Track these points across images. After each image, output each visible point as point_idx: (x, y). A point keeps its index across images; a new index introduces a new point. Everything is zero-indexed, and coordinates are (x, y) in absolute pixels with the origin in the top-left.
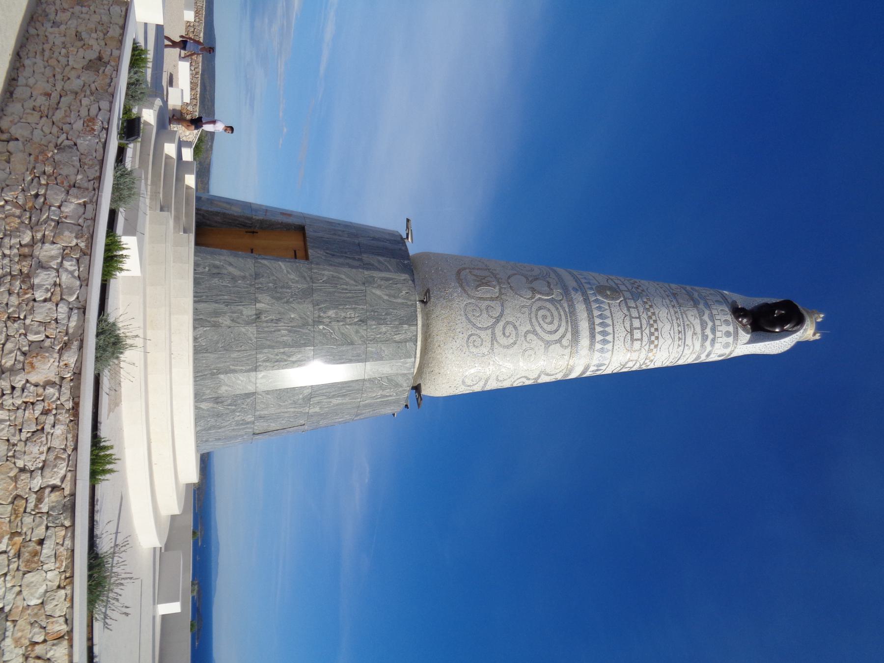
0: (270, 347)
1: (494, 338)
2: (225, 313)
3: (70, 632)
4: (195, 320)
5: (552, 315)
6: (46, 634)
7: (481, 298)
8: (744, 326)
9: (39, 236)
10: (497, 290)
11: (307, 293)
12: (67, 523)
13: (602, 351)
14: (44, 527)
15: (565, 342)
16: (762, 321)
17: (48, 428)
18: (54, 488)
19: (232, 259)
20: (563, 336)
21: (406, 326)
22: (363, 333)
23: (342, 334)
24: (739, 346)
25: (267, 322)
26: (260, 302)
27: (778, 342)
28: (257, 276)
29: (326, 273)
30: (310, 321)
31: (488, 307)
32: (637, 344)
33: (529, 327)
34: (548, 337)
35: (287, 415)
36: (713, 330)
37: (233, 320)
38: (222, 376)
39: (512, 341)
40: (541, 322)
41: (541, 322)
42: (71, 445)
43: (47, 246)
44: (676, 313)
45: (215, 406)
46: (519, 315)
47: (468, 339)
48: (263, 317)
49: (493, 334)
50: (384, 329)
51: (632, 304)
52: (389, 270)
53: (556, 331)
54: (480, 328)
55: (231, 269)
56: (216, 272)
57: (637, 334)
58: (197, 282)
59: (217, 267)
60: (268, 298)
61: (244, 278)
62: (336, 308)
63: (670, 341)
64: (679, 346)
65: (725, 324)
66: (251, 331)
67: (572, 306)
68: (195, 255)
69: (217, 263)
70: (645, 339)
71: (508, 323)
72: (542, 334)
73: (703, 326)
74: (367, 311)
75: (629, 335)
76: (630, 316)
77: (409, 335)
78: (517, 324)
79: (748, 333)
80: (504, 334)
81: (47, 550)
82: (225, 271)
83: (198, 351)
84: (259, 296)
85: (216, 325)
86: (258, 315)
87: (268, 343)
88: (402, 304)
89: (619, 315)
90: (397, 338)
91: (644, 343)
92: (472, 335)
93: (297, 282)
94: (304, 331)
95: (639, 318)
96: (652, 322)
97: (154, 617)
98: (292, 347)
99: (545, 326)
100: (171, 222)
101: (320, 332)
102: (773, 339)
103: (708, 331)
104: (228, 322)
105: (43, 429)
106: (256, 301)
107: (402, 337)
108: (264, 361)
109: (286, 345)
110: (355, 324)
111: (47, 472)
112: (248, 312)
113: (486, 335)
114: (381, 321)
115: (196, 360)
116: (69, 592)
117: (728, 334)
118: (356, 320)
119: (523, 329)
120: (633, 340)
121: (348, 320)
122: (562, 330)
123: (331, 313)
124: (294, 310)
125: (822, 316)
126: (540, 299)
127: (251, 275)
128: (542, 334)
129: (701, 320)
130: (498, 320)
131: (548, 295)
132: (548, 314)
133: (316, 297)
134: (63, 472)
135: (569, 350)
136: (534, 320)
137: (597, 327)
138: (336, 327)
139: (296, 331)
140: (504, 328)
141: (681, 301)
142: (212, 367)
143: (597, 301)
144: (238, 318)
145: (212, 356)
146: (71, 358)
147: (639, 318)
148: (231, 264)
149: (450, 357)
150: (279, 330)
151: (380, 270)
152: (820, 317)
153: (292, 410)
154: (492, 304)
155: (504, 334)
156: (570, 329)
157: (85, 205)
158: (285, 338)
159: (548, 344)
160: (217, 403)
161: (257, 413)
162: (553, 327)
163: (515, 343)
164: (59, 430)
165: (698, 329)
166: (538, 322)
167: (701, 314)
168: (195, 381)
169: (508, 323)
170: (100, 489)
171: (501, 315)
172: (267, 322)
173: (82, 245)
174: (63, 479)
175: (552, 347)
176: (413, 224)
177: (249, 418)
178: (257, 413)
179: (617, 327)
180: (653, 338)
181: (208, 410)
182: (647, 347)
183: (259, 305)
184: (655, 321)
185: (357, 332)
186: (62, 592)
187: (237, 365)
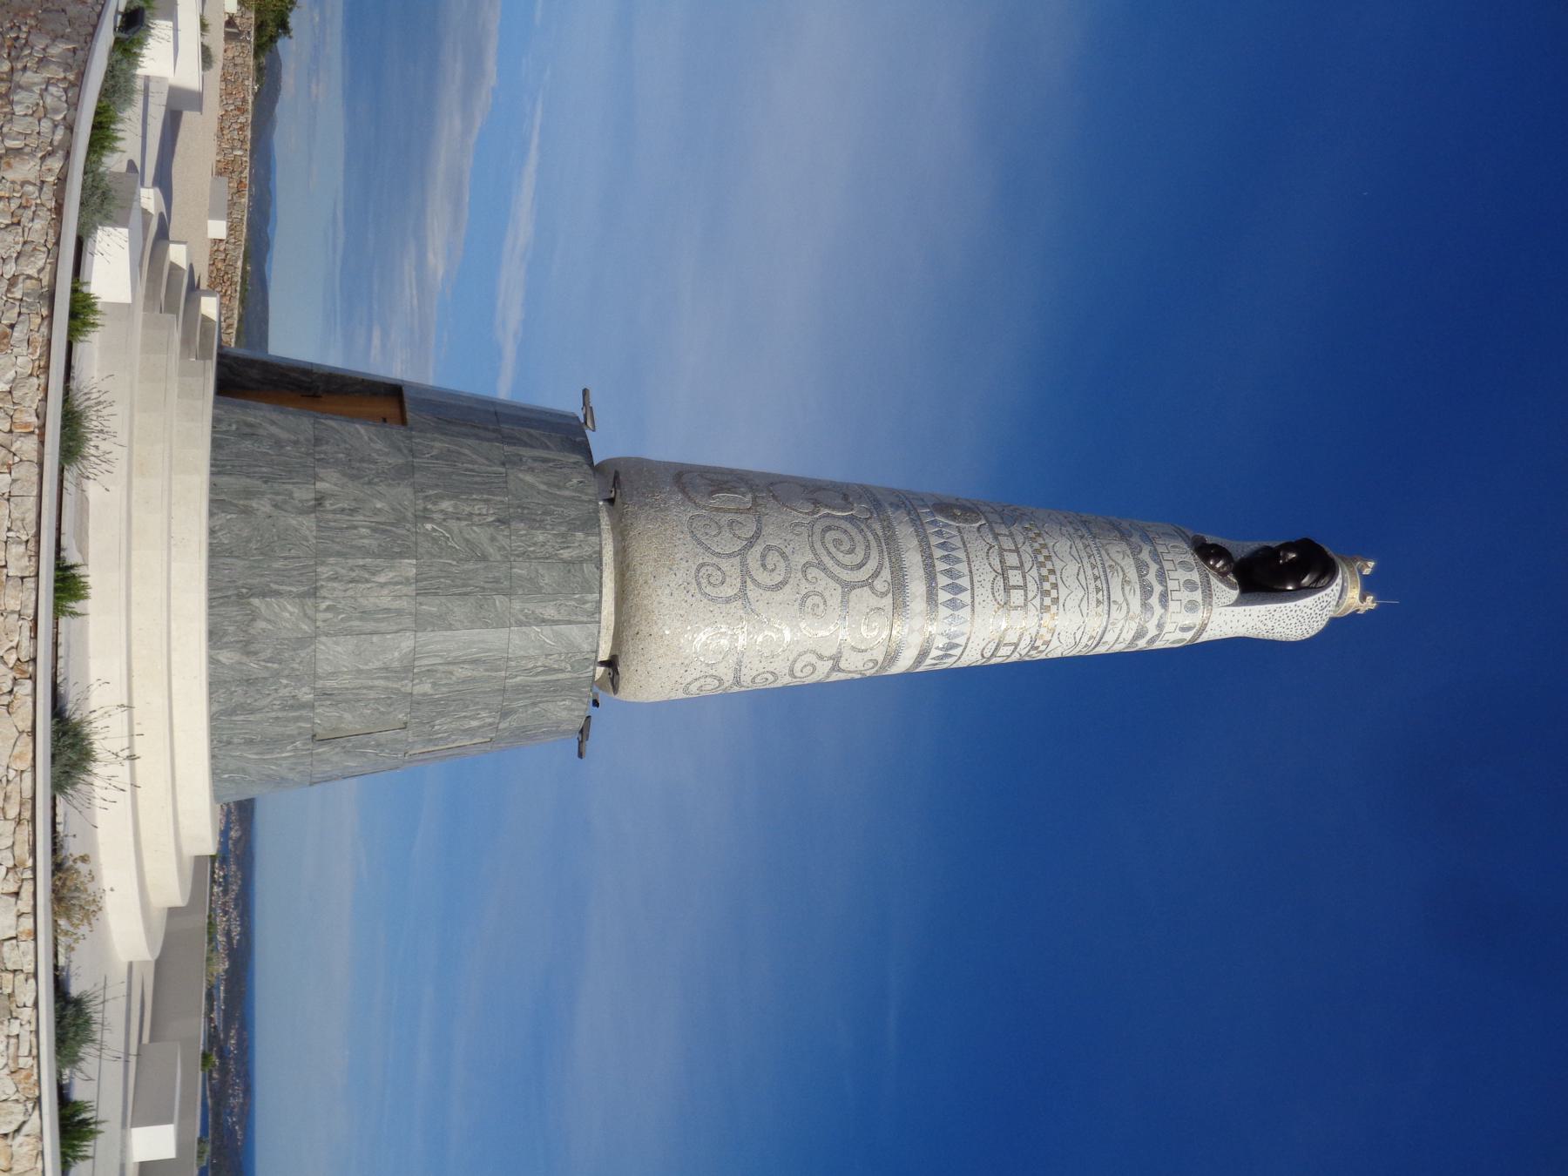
0: (339, 554)
1: (745, 572)
2: (263, 494)
3: (42, 427)
4: (212, 501)
5: (852, 539)
6: (12, 423)
7: (717, 509)
8: (1222, 575)
9: (20, 66)
10: (749, 497)
11: (404, 473)
12: (45, 312)
13: (953, 605)
14: (16, 310)
15: (880, 585)
16: (1261, 577)
17: (24, 221)
18: (29, 277)
19: (275, 416)
20: (876, 574)
21: (580, 535)
22: (505, 542)
23: (467, 540)
24: (1216, 610)
25: (334, 512)
26: (322, 480)
27: (1291, 605)
28: (318, 441)
29: (437, 444)
30: (409, 515)
31: (731, 523)
32: (1017, 597)
33: (809, 557)
34: (846, 576)
35: (372, 694)
36: (1162, 576)
37: (275, 506)
38: (256, 601)
39: (780, 579)
40: (833, 550)
41: (833, 550)
42: (52, 240)
43: (29, 74)
44: (1086, 547)
45: (245, 659)
46: (790, 537)
47: (698, 571)
48: (327, 503)
49: (743, 564)
50: (540, 537)
51: (1003, 530)
52: (547, 448)
53: (860, 566)
54: (719, 555)
55: (274, 430)
56: (249, 432)
57: (1015, 578)
58: (217, 445)
59: (251, 425)
60: (337, 475)
61: (296, 443)
62: (455, 497)
63: (1081, 593)
64: (1098, 602)
65: (1183, 570)
66: (307, 524)
67: (888, 527)
68: (215, 407)
69: (251, 419)
70: (1032, 587)
71: (769, 548)
72: (837, 570)
73: (1141, 567)
74: (509, 506)
75: (1000, 578)
76: (1000, 547)
77: (587, 551)
78: (788, 551)
79: (1232, 587)
80: (764, 566)
81: (18, 334)
82: (261, 431)
83: (216, 553)
84: (321, 472)
85: (247, 512)
86: (320, 500)
87: (338, 548)
88: (572, 498)
89: (978, 546)
90: (565, 554)
91: (1031, 595)
92: (703, 565)
93: (387, 454)
94: (400, 531)
95: (1017, 551)
96: (1041, 559)
97: (123, 1167)
98: (379, 556)
99: (840, 556)
100: (177, 336)
101: (426, 534)
102: (1285, 600)
103: (1151, 577)
104: (268, 509)
105: (19, 223)
106: (316, 477)
107: (575, 553)
108: (330, 579)
109: (367, 552)
110: (489, 524)
111: (22, 260)
112: (303, 494)
113: (731, 567)
114: (534, 522)
115: (212, 567)
116: (42, 381)
117: (1189, 585)
118: (490, 519)
119: (799, 560)
120: (1007, 589)
121: (476, 519)
122: (872, 565)
123: (446, 505)
124: (380, 496)
125: (1371, 564)
126: (828, 515)
127: (308, 440)
128: (837, 570)
129: (1136, 560)
130: (751, 542)
131: (843, 510)
132: (844, 537)
133: (419, 477)
134: (41, 264)
135: (888, 600)
136: (818, 545)
137: (937, 563)
138: (456, 530)
139: (384, 531)
140: (763, 556)
141: (1095, 530)
142: (240, 583)
143: (934, 523)
144: (285, 502)
145: (242, 563)
146: (56, 164)
147: (1017, 551)
148: (273, 423)
149: (666, 601)
150: (355, 527)
151: (532, 447)
152: (1369, 567)
153: (382, 683)
154: (740, 518)
155: (764, 566)
156: (887, 563)
157: (74, 51)
158: (366, 541)
159: (848, 587)
160: (248, 654)
161: (319, 684)
162: (858, 558)
163: (784, 583)
164: (38, 225)
165: (1132, 574)
166: (829, 553)
167: (1135, 552)
168: (210, 607)
169: (769, 548)
170: (79, 348)
171: (757, 535)
172: (334, 512)
173: (71, 77)
174: (40, 271)
175: (857, 591)
176: (594, 401)
177: (306, 695)
178: (319, 684)
179: (976, 565)
180: (1047, 586)
181: (231, 667)
182: (1037, 602)
183: (320, 485)
184: (1048, 558)
185: (493, 539)
186: (35, 380)
187: (282, 583)
